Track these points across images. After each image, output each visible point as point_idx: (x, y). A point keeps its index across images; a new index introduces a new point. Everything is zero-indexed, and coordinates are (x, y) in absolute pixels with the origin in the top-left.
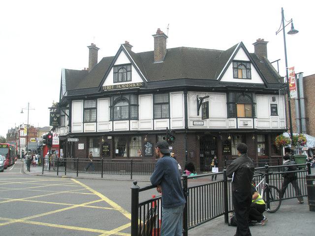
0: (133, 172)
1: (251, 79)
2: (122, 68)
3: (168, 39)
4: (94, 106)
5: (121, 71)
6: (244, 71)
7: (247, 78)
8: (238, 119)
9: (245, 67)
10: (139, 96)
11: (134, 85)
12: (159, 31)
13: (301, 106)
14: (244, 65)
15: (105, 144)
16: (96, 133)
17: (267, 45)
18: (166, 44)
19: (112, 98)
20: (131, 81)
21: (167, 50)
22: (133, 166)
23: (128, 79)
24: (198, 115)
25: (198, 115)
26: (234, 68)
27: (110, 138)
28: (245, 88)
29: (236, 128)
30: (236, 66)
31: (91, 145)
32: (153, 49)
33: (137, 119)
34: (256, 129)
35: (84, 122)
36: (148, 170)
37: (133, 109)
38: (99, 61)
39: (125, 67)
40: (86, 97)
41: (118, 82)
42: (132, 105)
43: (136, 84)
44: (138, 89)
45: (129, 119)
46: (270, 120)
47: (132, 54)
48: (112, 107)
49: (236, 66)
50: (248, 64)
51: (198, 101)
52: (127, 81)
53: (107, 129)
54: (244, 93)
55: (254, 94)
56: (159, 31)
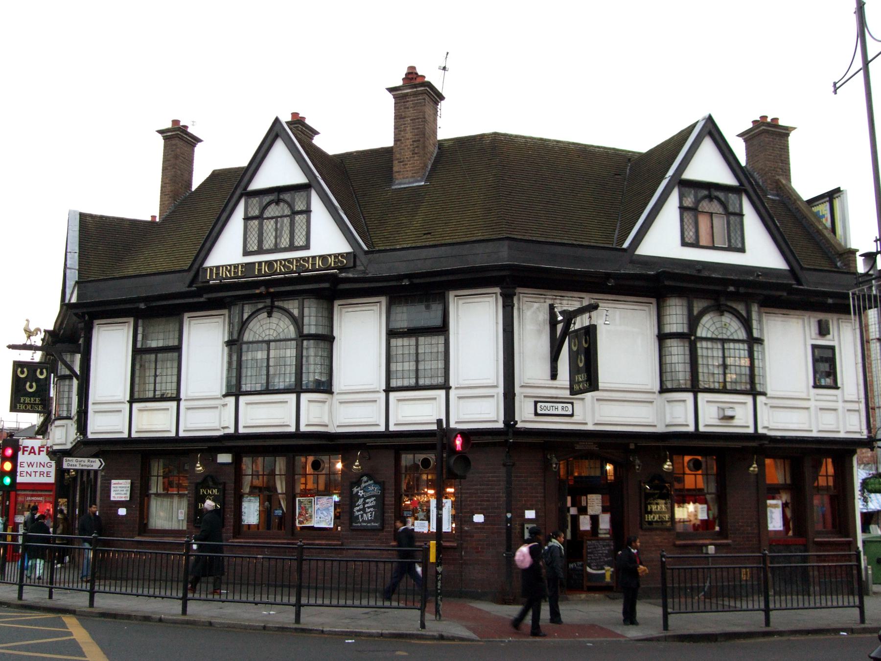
0: (304, 592)
1: (742, 250)
2: (278, 202)
3: (443, 106)
4: (173, 342)
5: (272, 211)
6: (719, 223)
7: (730, 249)
8: (700, 396)
9: (724, 205)
10: (337, 303)
11: (319, 263)
12: (412, 76)
13: (262, 428)
14: (718, 199)
15: (206, 481)
16: (177, 440)
17: (790, 138)
18: (435, 120)
19: (236, 310)
20: (307, 247)
21: (441, 144)
22: (305, 567)
23: (300, 241)
24: (554, 376)
25: (554, 376)
26: (682, 209)
27: (224, 458)
28: (725, 282)
29: (691, 428)
30: (689, 202)
31: (157, 485)
32: (387, 141)
33: (325, 387)
34: (764, 437)
35: (132, 401)
36: (372, 587)
37: (311, 350)
38: (197, 182)
39: (286, 196)
40: (142, 306)
41: (260, 251)
42: (310, 337)
43: (324, 258)
44: (333, 278)
45: (298, 389)
46: (812, 404)
47: (317, 155)
48: (234, 344)
49: (689, 202)
50: (732, 197)
51: (553, 323)
52: (292, 248)
53: (216, 425)
54: (723, 301)
55: (755, 308)
56: (412, 76)
